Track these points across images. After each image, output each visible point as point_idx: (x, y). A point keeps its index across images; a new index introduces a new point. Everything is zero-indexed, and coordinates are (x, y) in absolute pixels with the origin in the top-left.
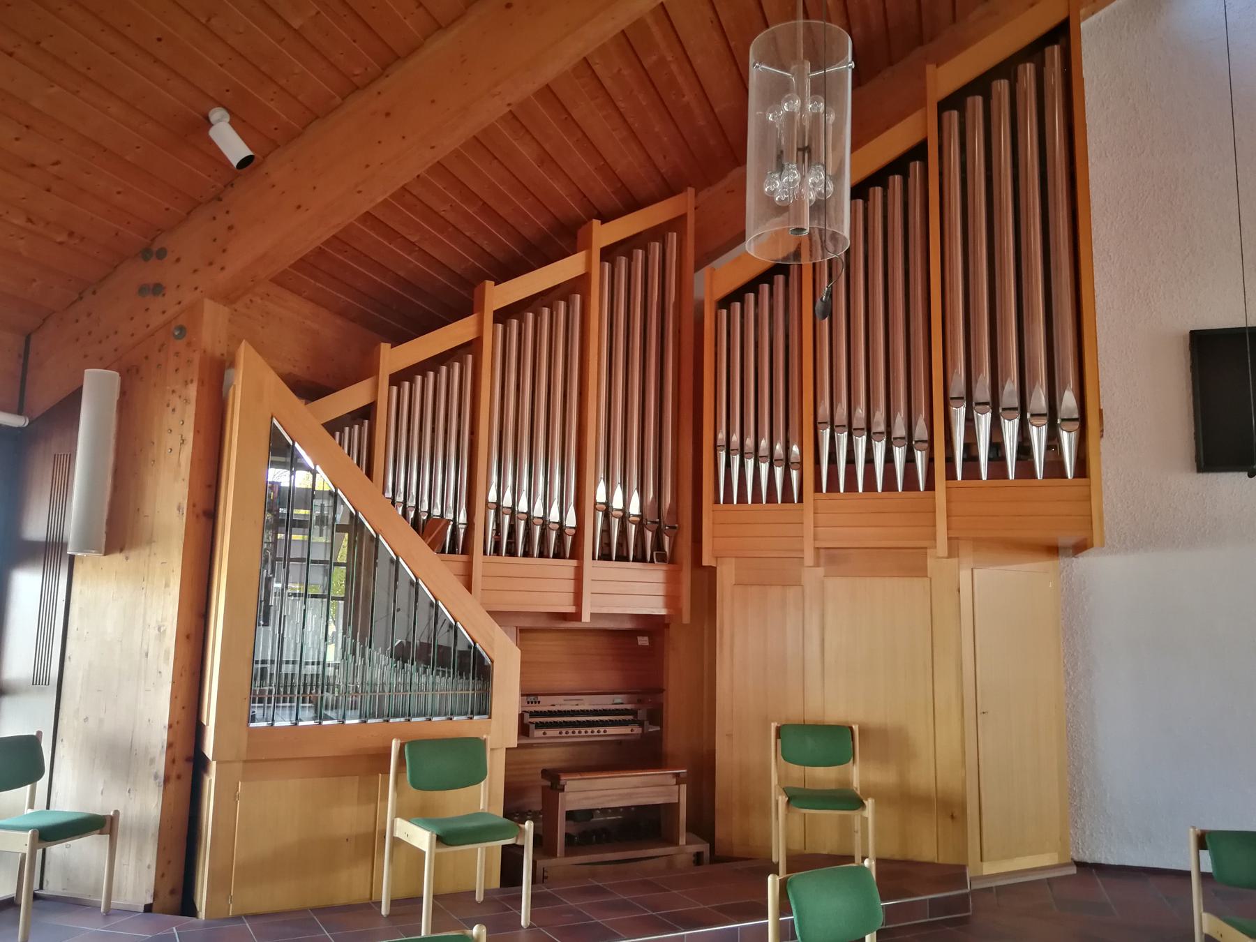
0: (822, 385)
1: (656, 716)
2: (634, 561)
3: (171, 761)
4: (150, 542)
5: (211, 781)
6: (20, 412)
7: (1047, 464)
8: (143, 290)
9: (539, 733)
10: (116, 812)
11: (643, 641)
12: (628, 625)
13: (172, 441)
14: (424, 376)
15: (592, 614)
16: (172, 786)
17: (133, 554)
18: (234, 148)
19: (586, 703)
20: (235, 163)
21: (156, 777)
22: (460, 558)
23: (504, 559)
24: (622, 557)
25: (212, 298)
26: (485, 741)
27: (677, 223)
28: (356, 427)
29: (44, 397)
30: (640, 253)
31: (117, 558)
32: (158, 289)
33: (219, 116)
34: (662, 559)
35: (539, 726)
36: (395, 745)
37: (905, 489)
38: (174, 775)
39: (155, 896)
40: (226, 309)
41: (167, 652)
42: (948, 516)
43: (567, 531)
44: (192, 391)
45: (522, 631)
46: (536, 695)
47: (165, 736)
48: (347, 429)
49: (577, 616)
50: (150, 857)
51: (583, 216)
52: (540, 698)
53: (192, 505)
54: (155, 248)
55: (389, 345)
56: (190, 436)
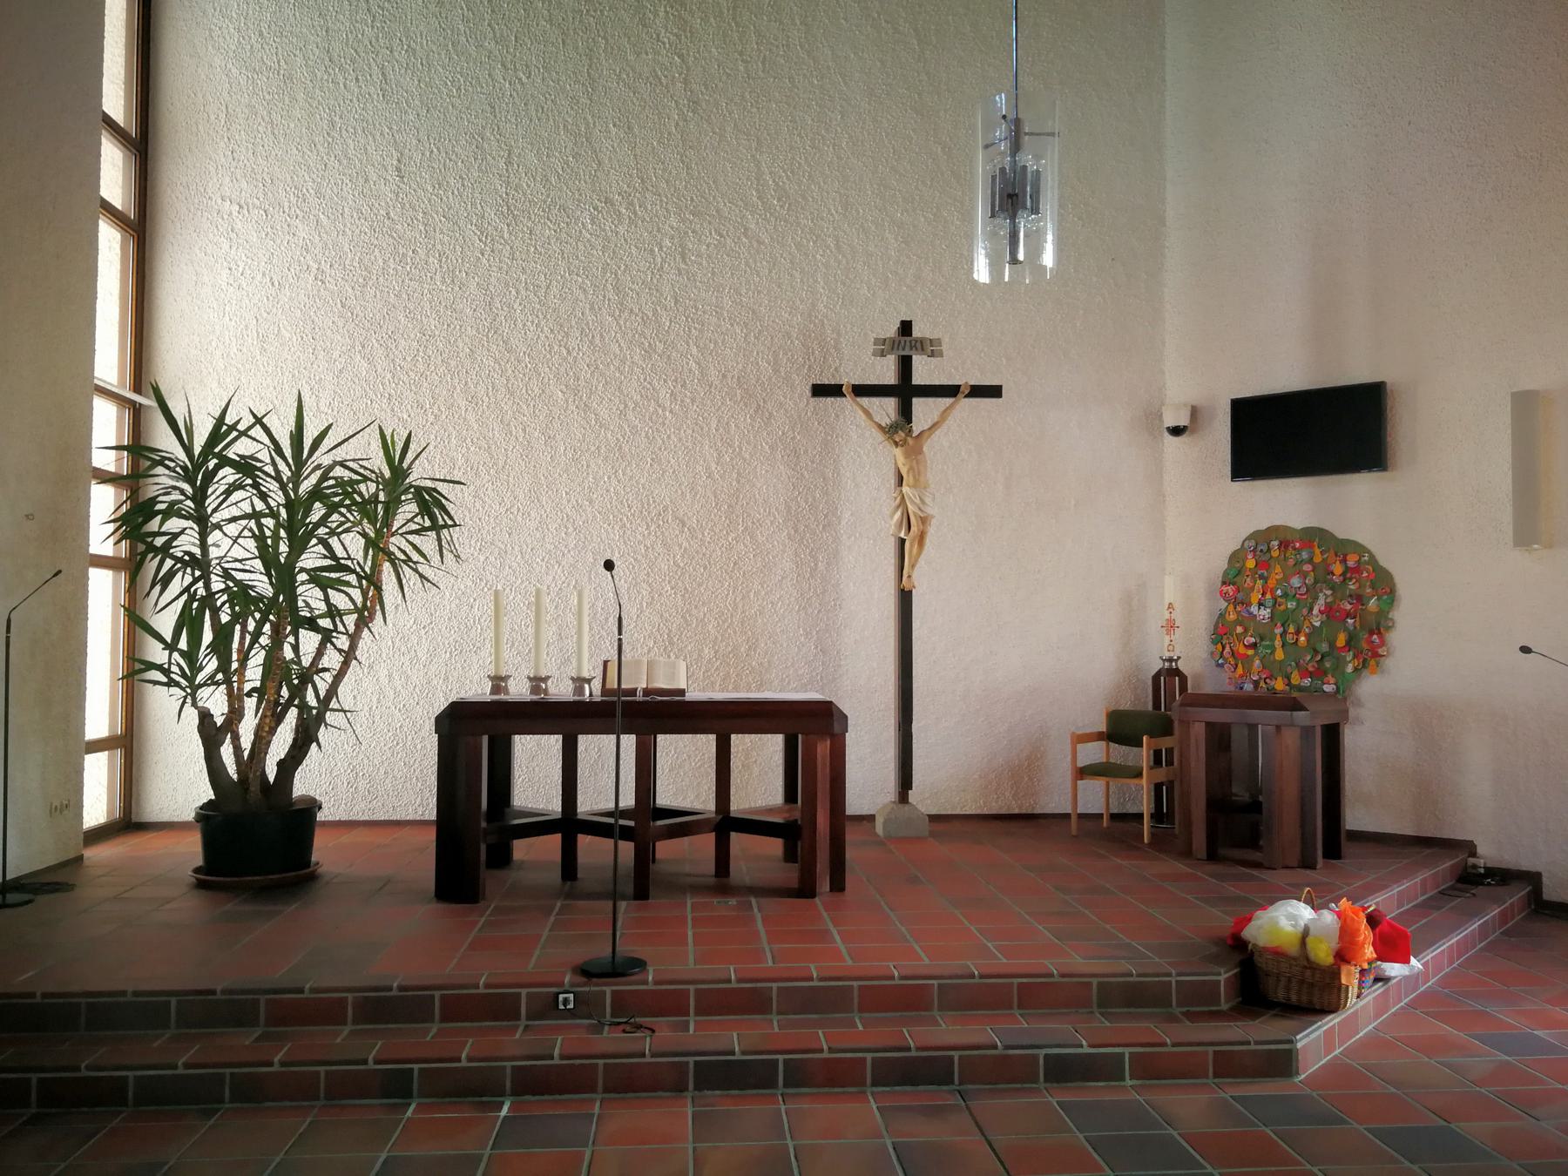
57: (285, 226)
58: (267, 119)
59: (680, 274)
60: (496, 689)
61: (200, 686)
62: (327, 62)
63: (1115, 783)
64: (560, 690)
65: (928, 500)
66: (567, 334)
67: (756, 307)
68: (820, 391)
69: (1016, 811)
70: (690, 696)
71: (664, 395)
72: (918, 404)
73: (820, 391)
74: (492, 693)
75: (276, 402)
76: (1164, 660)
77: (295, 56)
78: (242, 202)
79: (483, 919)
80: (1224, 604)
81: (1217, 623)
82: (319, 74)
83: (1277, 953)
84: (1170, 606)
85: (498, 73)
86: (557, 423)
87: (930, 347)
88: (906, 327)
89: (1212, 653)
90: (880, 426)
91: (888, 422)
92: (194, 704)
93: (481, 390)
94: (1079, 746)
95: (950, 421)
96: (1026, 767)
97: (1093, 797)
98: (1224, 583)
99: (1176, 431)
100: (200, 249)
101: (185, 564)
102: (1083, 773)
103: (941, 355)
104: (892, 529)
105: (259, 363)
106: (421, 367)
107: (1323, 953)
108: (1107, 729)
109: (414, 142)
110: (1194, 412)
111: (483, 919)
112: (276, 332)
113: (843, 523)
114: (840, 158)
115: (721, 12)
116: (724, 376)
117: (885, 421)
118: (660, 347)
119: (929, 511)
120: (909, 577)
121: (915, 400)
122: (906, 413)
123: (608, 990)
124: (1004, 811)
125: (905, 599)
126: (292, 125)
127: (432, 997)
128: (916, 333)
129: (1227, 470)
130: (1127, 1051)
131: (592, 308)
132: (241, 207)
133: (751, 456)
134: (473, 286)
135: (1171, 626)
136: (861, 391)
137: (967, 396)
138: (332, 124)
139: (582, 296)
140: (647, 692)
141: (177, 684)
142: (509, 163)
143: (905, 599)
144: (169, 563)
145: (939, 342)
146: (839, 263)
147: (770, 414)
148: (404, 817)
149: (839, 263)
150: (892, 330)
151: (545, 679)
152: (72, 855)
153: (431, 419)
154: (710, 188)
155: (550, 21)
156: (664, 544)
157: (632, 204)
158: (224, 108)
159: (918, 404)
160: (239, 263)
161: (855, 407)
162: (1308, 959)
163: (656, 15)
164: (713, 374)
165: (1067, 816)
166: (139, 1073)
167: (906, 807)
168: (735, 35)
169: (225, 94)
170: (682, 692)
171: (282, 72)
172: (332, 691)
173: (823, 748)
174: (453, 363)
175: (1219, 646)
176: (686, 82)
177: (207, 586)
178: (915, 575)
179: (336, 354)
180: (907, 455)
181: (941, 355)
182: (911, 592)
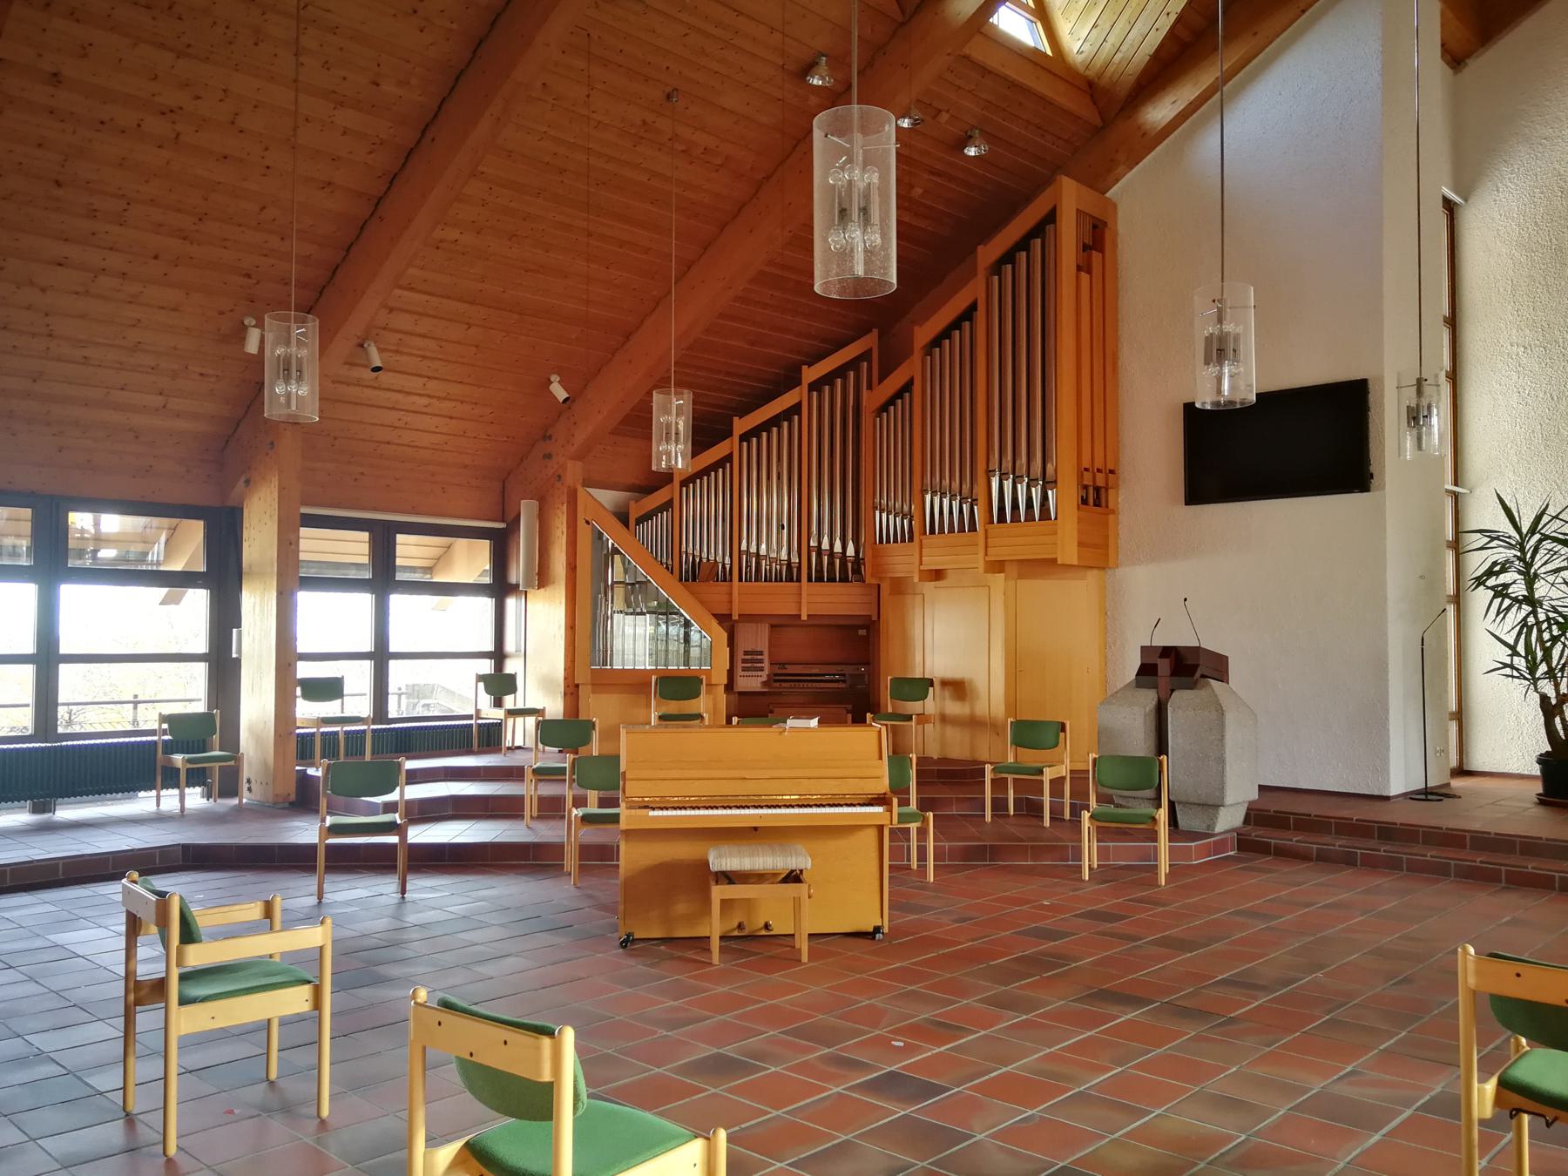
2: (786, 581)
4: (554, 583)
6: (503, 521)
9: (777, 684)
11: (862, 632)
13: (558, 533)
15: (808, 616)
17: (548, 589)
18: (560, 393)
20: (561, 401)
24: (832, 579)
25: (572, 459)
27: (866, 356)
31: (542, 590)
33: (555, 378)
40: (581, 463)
43: (793, 565)
46: (784, 664)
49: (799, 616)
51: (830, 347)
54: (548, 434)
57: (1561, 356)
58: (1543, 283)
61: (1539, 679)
75: (1558, 481)
77: (1563, 233)
78: (1526, 345)
92: (1536, 690)
100: (1496, 382)
101: (1520, 602)
105: (1545, 455)
108: (565, 714)
112: (1556, 432)
126: (1563, 283)
132: (1525, 348)
141: (1525, 678)
144: (1507, 602)
152: (1445, 782)
158: (1510, 282)
160: (1526, 387)
166: (1562, 875)
169: (1511, 272)
171: (1553, 247)
177: (1536, 617)
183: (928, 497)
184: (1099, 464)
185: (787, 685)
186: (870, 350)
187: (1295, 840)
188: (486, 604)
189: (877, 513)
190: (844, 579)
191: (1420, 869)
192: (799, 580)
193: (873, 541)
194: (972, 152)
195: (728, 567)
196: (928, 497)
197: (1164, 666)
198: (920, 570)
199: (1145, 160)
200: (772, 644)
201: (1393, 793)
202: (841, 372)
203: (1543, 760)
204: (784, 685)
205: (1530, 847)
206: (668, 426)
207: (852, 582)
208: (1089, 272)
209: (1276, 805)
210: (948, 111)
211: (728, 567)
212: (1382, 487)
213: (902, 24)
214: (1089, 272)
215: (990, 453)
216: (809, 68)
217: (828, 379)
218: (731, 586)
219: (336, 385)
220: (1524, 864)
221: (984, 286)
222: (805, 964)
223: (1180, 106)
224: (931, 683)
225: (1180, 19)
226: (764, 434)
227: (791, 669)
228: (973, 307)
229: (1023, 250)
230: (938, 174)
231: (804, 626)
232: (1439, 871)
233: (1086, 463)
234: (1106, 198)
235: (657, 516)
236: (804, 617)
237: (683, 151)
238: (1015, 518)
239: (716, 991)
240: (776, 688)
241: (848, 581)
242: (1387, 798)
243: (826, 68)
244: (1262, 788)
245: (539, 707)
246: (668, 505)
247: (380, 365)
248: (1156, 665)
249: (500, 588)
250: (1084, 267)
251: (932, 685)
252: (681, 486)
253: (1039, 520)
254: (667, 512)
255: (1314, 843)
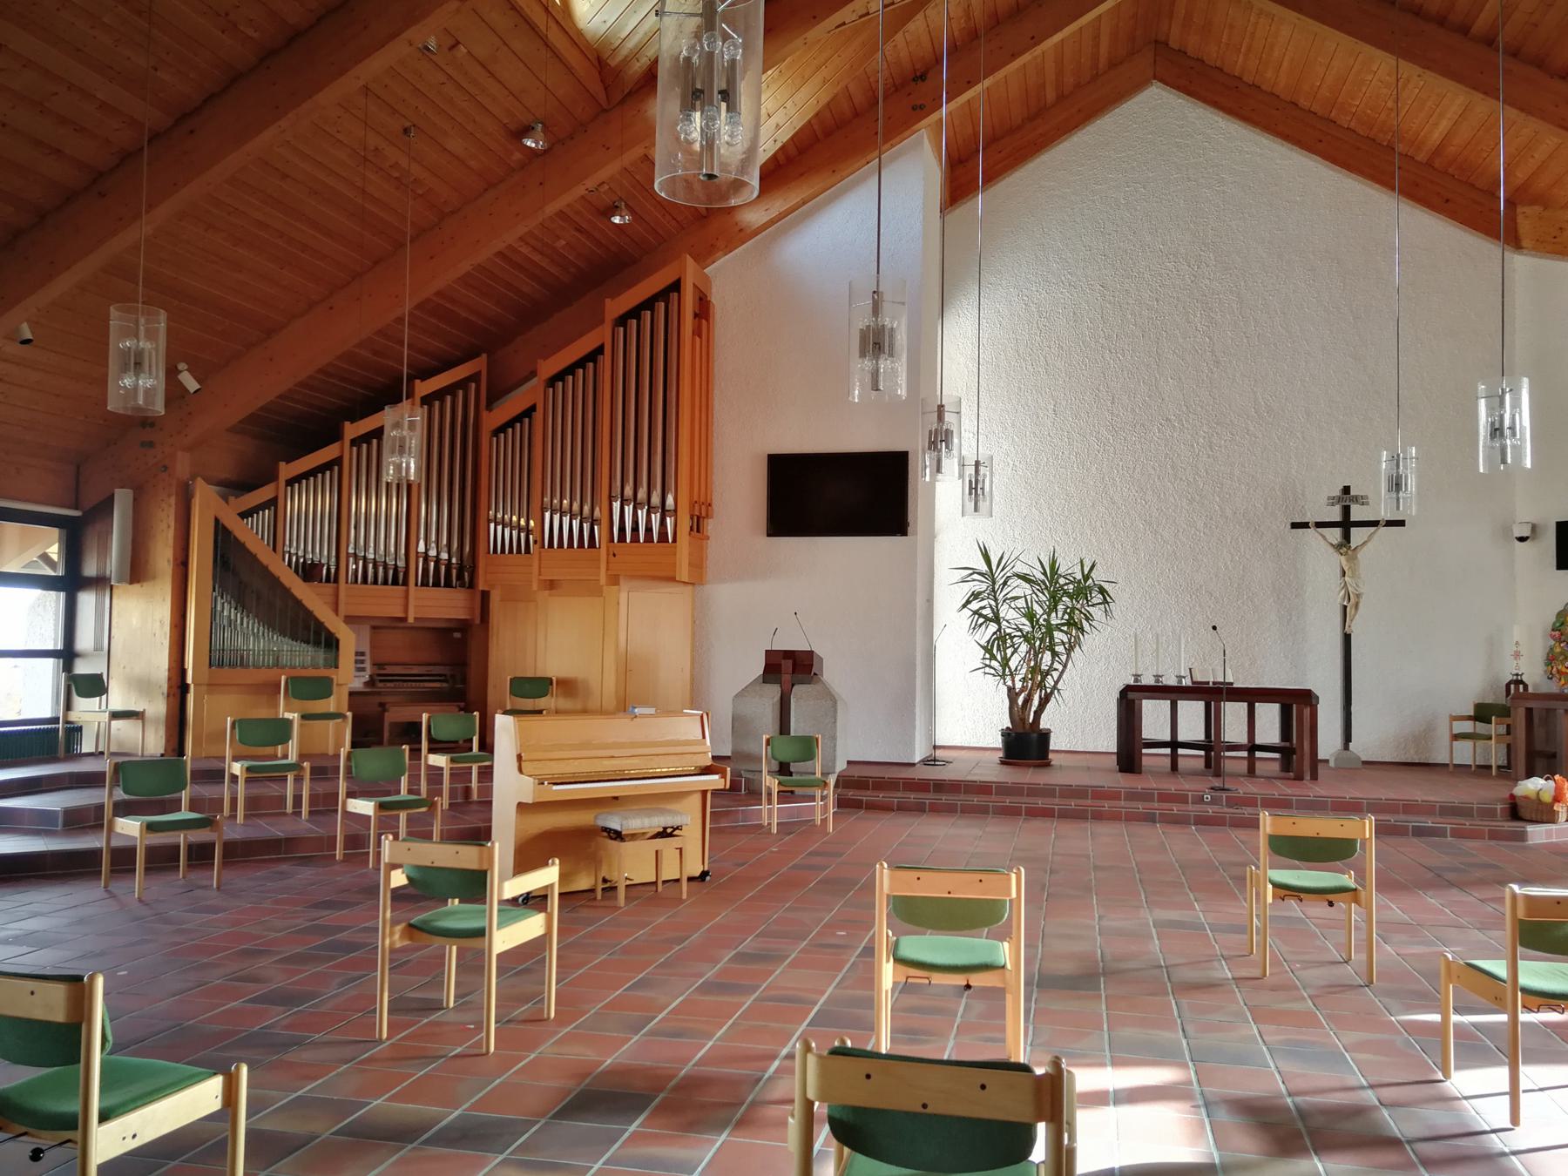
0: (642, 460)
1: (464, 680)
3: (170, 687)
4: (154, 578)
5: (191, 698)
6: (76, 508)
7: (660, 533)
8: (143, 444)
9: (381, 685)
10: (144, 710)
11: (457, 635)
12: (443, 625)
14: (315, 477)
15: (415, 618)
16: (171, 698)
17: (145, 584)
19: (415, 670)
21: (163, 694)
22: (402, 588)
23: (360, 586)
24: (437, 584)
26: (332, 680)
27: (475, 377)
28: (267, 511)
29: (92, 498)
30: (437, 404)
31: (136, 587)
32: (151, 444)
34: (463, 585)
35: (381, 681)
36: (283, 678)
37: (525, 553)
38: (172, 693)
39: (165, 750)
41: (165, 634)
42: (608, 563)
43: (399, 569)
44: (173, 500)
45: (374, 628)
47: (167, 673)
48: (261, 512)
49: (404, 619)
50: (162, 732)
51: (442, 346)
52: (386, 667)
53: (175, 559)
55: (284, 463)
56: (172, 524)
59: (1209, 457)
60: (1136, 680)
62: (1017, 357)
63: (1480, 743)
64: (1171, 681)
65: (1361, 586)
66: (1145, 494)
67: (1254, 473)
68: (1295, 526)
69: (1417, 761)
70: (1235, 686)
71: (1200, 524)
72: (1353, 530)
73: (1295, 526)
74: (1134, 682)
76: (1514, 675)
79: (636, 1038)
80: (1553, 642)
81: (1548, 654)
82: (1013, 363)
83: (1526, 797)
84: (1517, 643)
85: (1107, 355)
86: (1140, 541)
87: (1361, 500)
88: (1346, 490)
89: (1545, 671)
90: (1332, 544)
91: (1336, 542)
93: (1098, 524)
94: (1454, 723)
95: (1376, 537)
96: (1424, 735)
97: (1464, 753)
98: (1553, 630)
99: (1522, 539)
102: (1456, 737)
103: (1368, 504)
104: (1339, 600)
106: (1066, 513)
107: (1547, 797)
109: (1063, 395)
110: (1534, 528)
111: (636, 1038)
113: (1308, 593)
114: (1305, 387)
115: (1233, 311)
116: (1235, 513)
117: (1335, 542)
118: (1198, 498)
119: (1361, 590)
120: (1350, 627)
121: (1352, 529)
122: (1347, 537)
123: (1224, 795)
124: (1409, 761)
125: (1347, 639)
127: (1154, 793)
128: (1353, 493)
129: (1555, 568)
130: (1449, 826)
131: (1159, 478)
133: (1251, 556)
134: (1094, 469)
135: (1517, 655)
136: (1319, 525)
137: (1385, 526)
138: (1020, 388)
139: (1153, 472)
140: (1214, 683)
142: (1113, 403)
143: (1347, 639)
144: (981, 620)
145: (1367, 497)
146: (1304, 446)
147: (1263, 533)
148: (1060, 749)
149: (1304, 446)
150: (1337, 492)
151: (1161, 676)
153: (1072, 540)
154: (1226, 409)
155: (1135, 325)
156: (1200, 606)
157: (1182, 420)
159: (1353, 530)
161: (1317, 534)
162: (1540, 800)
163: (1195, 316)
164: (1229, 512)
165: (1447, 765)
167: (1349, 752)
168: (1242, 323)
170: (1232, 684)
172: (1056, 683)
173: (1307, 711)
174: (1083, 510)
175: (1550, 667)
176: (1212, 351)
178: (1352, 625)
179: (1023, 508)
180: (1347, 561)
181: (1368, 504)
182: (1350, 635)
183: (547, 515)
184: (702, 500)
185: (391, 685)
186: (480, 372)
187: (881, 796)
188: (54, 601)
189: (492, 525)
190: (448, 584)
191: (968, 811)
192: (405, 583)
193: (486, 551)
194: (617, 220)
195: (333, 571)
196: (547, 515)
197: (787, 665)
198: (539, 580)
199: (736, 251)
200: (373, 647)
201: (916, 762)
202: (451, 389)
203: (1006, 734)
204: (389, 684)
205: (1003, 789)
206: (402, 439)
207: (456, 587)
208: (700, 336)
209: (857, 772)
210: (608, 184)
211: (333, 571)
212: (915, 533)
213: (605, 111)
214: (700, 336)
215: (613, 480)
216: (526, 131)
217: (439, 395)
218: (338, 588)
219: (994, 514)
220: (1036, 802)
221: (610, 333)
222: (686, 901)
223: (773, 213)
224: (550, 681)
225: (783, 148)
226: (375, 441)
227: (390, 670)
228: (600, 350)
229: (648, 310)
230: (579, 230)
231: (412, 628)
232: (982, 811)
233: (696, 499)
234: (705, 273)
235: (258, 514)
236: (411, 620)
237: (396, 178)
238: (635, 538)
239: (665, 917)
240: (381, 688)
241: (452, 587)
242: (914, 765)
243: (542, 134)
244: (849, 762)
245: (139, 708)
246: (272, 503)
247: (31, 338)
248: (780, 665)
249: (71, 582)
250: (697, 332)
251: (551, 684)
252: (287, 486)
253: (658, 542)
254: (269, 509)
255: (896, 797)
